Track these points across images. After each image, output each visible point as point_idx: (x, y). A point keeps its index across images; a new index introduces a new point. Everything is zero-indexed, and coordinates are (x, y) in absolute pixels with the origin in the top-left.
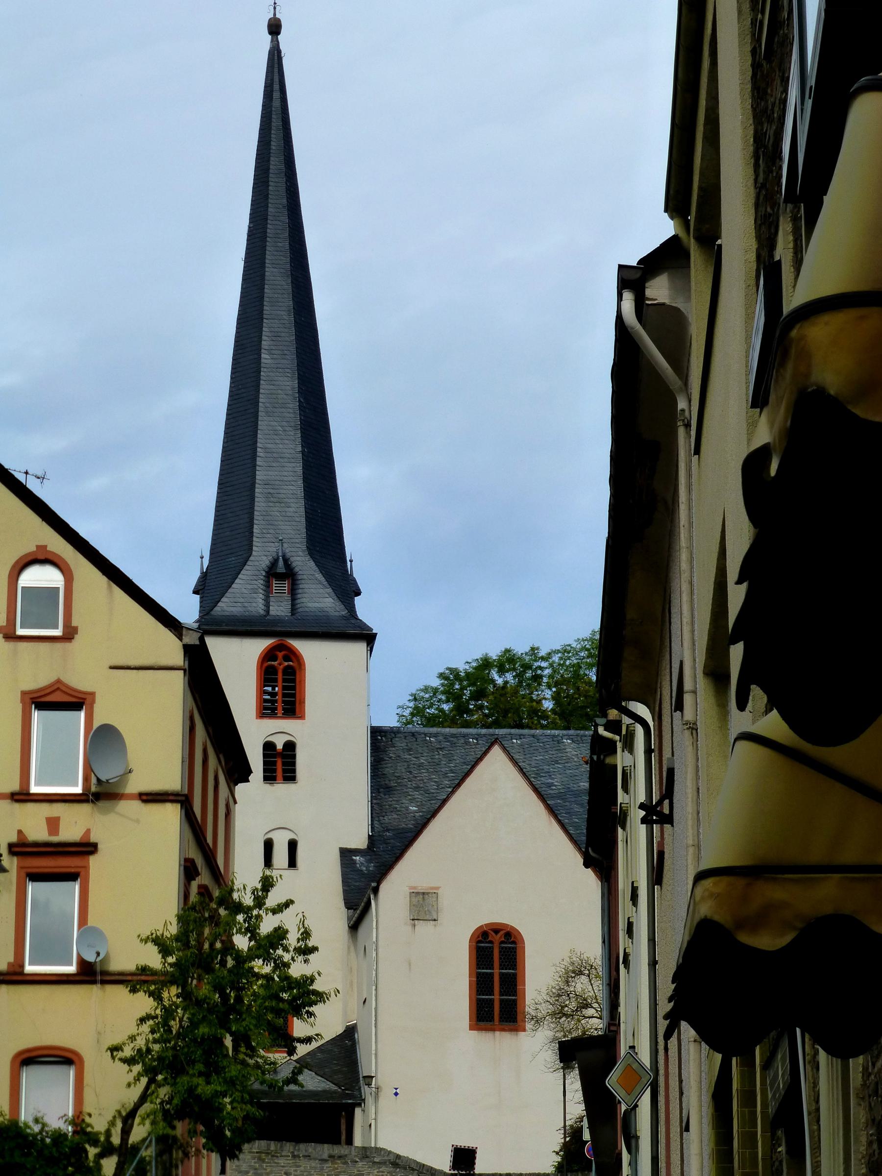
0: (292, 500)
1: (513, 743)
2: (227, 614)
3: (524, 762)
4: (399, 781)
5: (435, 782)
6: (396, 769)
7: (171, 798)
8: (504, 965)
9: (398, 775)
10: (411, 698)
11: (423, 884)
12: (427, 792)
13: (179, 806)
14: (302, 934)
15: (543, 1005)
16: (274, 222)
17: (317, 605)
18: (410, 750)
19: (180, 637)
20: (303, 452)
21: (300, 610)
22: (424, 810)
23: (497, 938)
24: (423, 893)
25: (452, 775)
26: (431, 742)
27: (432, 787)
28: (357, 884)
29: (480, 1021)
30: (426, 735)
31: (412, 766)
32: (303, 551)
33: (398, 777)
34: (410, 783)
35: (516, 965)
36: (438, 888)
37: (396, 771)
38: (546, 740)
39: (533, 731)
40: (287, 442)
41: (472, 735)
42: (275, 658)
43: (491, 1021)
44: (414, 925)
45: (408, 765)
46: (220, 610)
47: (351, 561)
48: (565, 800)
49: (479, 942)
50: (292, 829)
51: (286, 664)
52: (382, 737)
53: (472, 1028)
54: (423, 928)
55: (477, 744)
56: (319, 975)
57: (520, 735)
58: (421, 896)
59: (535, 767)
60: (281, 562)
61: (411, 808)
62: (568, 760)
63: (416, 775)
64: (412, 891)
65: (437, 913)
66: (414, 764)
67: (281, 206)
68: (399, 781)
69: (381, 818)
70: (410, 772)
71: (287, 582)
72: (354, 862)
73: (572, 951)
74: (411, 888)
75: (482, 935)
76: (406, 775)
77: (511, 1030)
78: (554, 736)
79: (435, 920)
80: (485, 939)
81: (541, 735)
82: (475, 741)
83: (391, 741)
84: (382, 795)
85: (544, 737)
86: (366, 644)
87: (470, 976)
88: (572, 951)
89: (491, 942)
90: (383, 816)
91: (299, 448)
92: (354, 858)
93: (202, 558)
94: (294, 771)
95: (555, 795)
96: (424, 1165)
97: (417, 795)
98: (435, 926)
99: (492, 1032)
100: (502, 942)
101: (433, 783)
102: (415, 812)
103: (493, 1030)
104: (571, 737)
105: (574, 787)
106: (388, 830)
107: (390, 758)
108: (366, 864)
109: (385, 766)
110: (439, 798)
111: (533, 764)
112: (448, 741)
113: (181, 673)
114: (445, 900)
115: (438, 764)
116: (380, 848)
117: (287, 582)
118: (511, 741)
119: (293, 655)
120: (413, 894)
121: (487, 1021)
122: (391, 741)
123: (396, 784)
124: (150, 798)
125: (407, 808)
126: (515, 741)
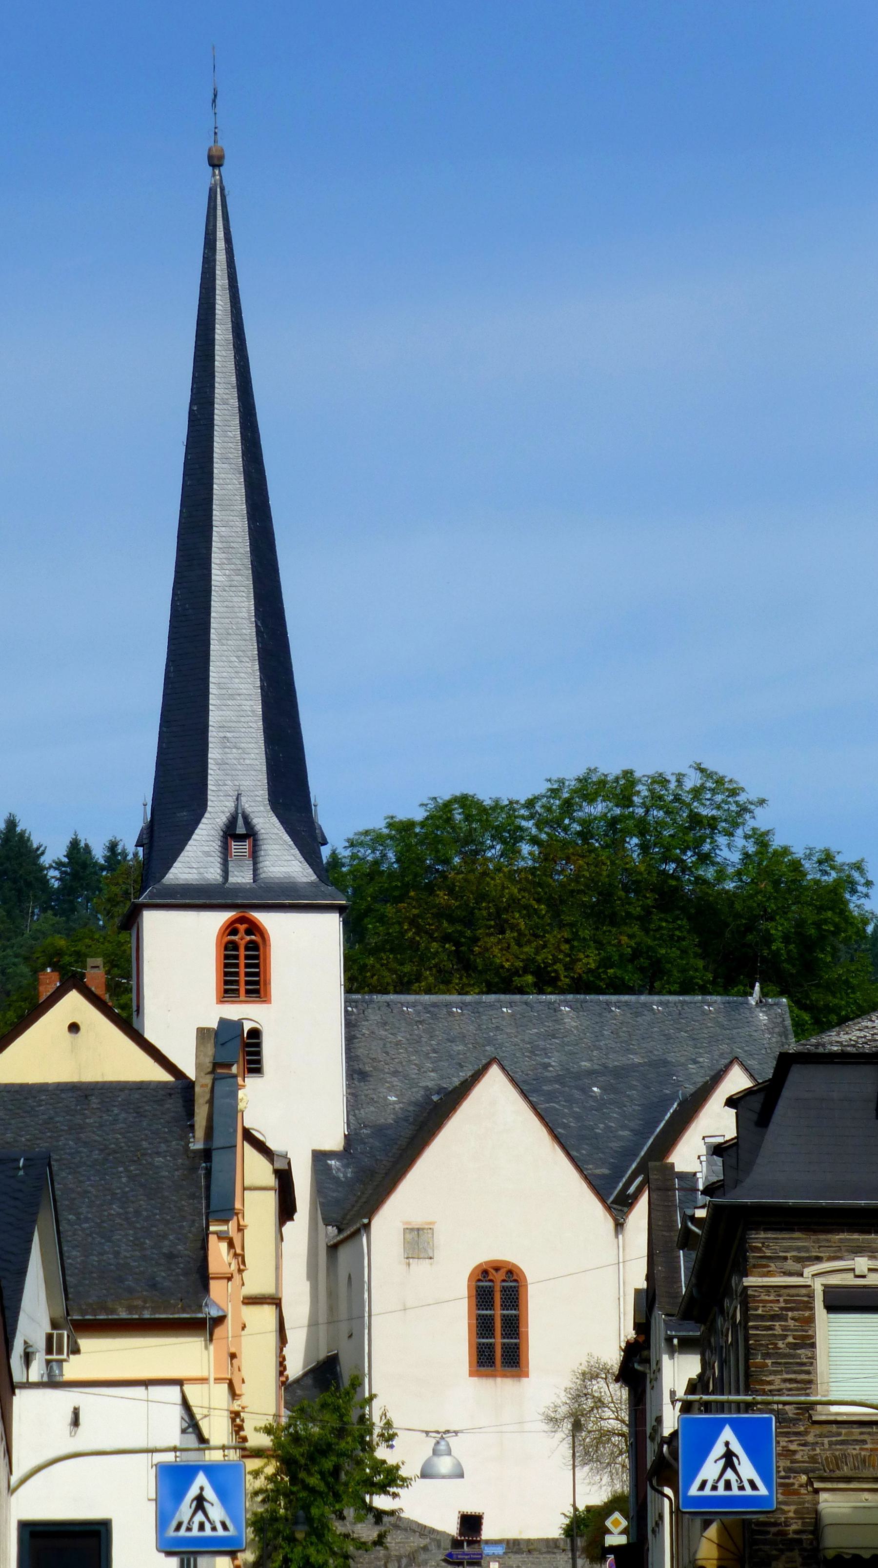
0: (250, 745)
1: (503, 1012)
2: (181, 882)
3: (516, 1037)
4: (375, 1064)
5: (415, 1064)
6: (370, 1049)
7: (268, 1301)
8: (505, 1305)
9: (373, 1057)
10: (347, 844)
11: (418, 1219)
12: (406, 1077)
13: (274, 1307)
14: (385, 1424)
15: (563, 1407)
16: (221, 407)
17: (283, 869)
18: (385, 1024)
19: (272, 1161)
20: (262, 687)
21: (262, 876)
22: (404, 1101)
23: (499, 1276)
24: (418, 1230)
25: (435, 1055)
26: (408, 1013)
27: (413, 1071)
28: (335, 1195)
29: (480, 1366)
30: (403, 1005)
31: (388, 1045)
32: (265, 806)
33: (373, 1059)
34: (387, 1067)
35: (517, 1306)
36: (431, 1223)
37: (372, 1052)
38: (540, 1007)
39: (525, 997)
40: (242, 675)
41: (455, 1003)
42: (234, 932)
43: (491, 1366)
44: (409, 1264)
45: (385, 1044)
46: (173, 877)
47: (315, 806)
48: (563, 1084)
49: (479, 1280)
50: (258, 1129)
51: (248, 938)
52: (352, 1008)
53: (472, 1374)
54: (420, 1267)
55: (462, 1014)
56: (403, 1464)
57: (510, 1003)
58: (416, 1233)
59: (529, 1043)
60: (240, 821)
61: (389, 1098)
62: (566, 1034)
63: (394, 1057)
64: (406, 1227)
65: (433, 1251)
66: (390, 1042)
67: (230, 387)
68: (375, 1064)
69: (357, 1112)
70: (387, 1053)
71: (247, 843)
72: (329, 1167)
73: (590, 1355)
74: (407, 1223)
75: (482, 1273)
76: (382, 1056)
77: (513, 1376)
78: (550, 1003)
79: (431, 1258)
80: (484, 1277)
81: (536, 1003)
82: (459, 1011)
83: (364, 1013)
84: (356, 1082)
85: (538, 1004)
86: (338, 915)
87: (469, 1318)
88: (590, 1355)
89: (491, 1281)
90: (359, 1110)
91: (258, 684)
92: (329, 1162)
93: (145, 805)
94: (259, 1062)
95: (552, 1079)
96: (425, 1527)
97: (395, 1081)
98: (431, 1264)
99: (494, 1379)
100: (504, 1281)
101: (414, 1067)
102: (395, 1103)
103: (494, 1376)
104: (569, 1003)
105: (575, 1068)
106: (365, 1126)
107: (363, 1035)
108: (343, 1170)
109: (358, 1045)
110: (420, 1085)
111: (527, 1039)
112: (429, 1012)
113: (272, 1193)
114: (442, 1237)
115: (418, 1042)
116: (356, 1149)
117: (247, 843)
118: (500, 1010)
119: (254, 928)
120: (408, 1231)
121: (488, 1366)
122: (364, 1013)
123: (371, 1069)
124: (250, 1301)
125: (385, 1098)
126: (505, 1010)
